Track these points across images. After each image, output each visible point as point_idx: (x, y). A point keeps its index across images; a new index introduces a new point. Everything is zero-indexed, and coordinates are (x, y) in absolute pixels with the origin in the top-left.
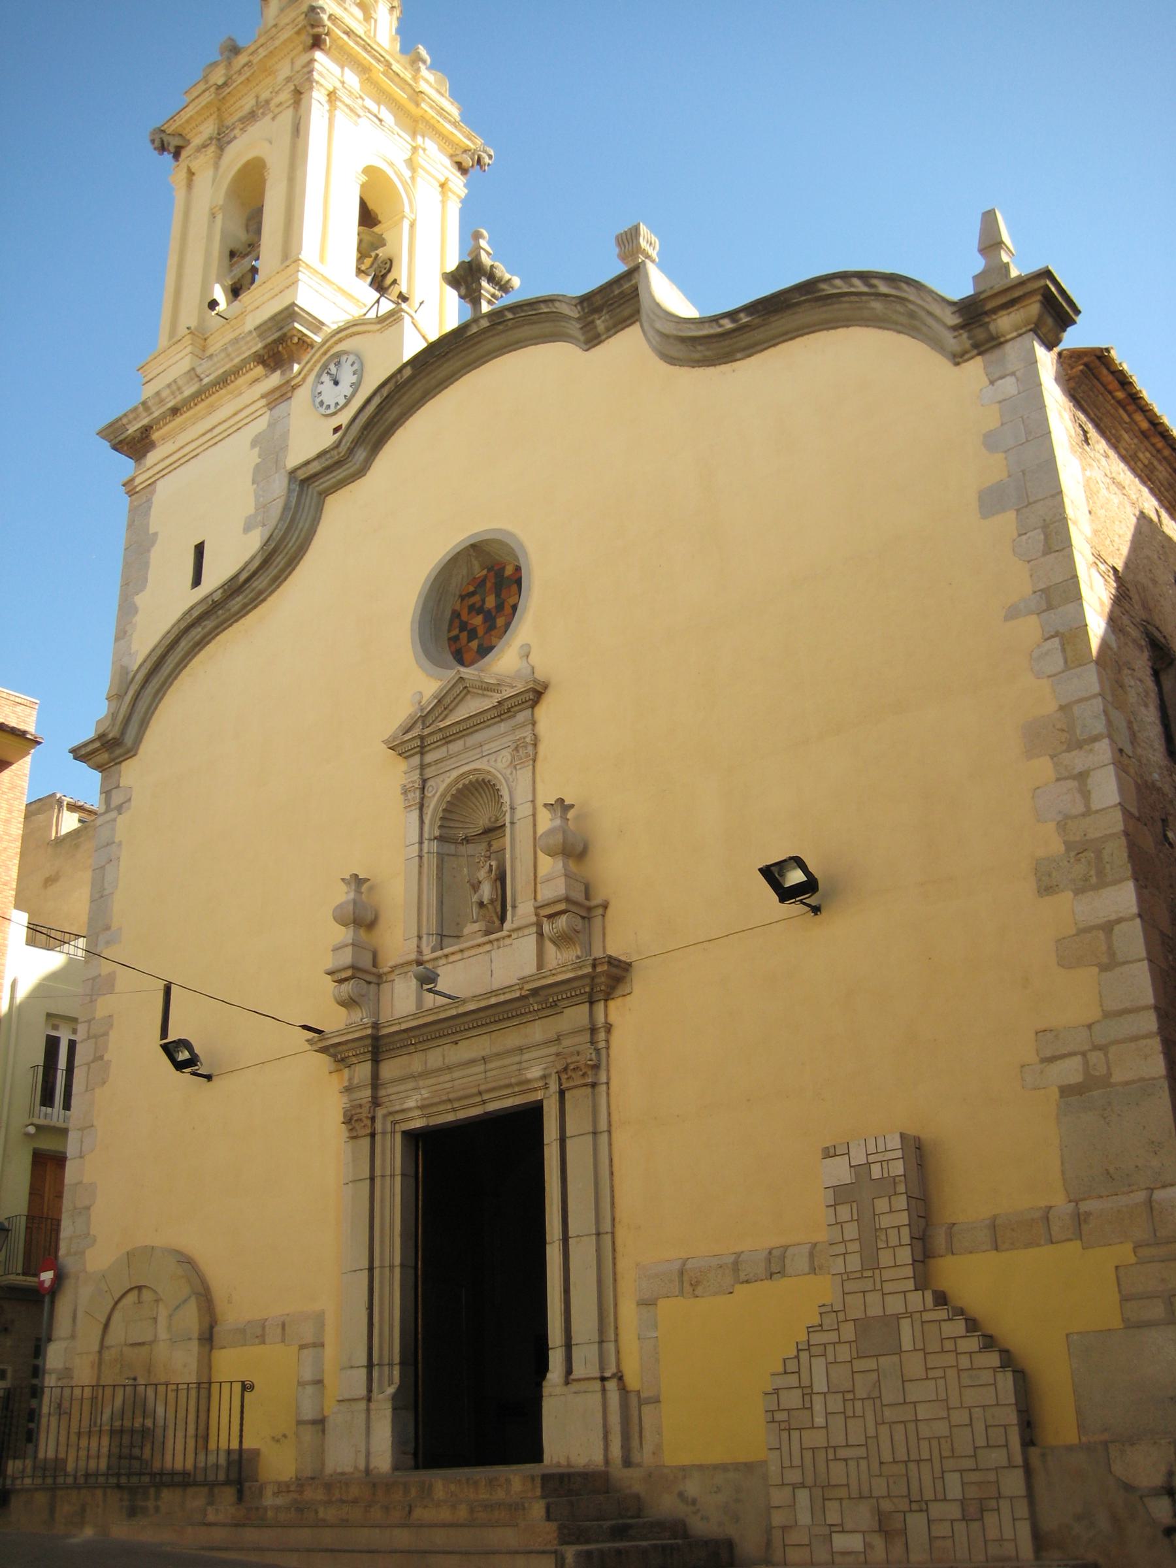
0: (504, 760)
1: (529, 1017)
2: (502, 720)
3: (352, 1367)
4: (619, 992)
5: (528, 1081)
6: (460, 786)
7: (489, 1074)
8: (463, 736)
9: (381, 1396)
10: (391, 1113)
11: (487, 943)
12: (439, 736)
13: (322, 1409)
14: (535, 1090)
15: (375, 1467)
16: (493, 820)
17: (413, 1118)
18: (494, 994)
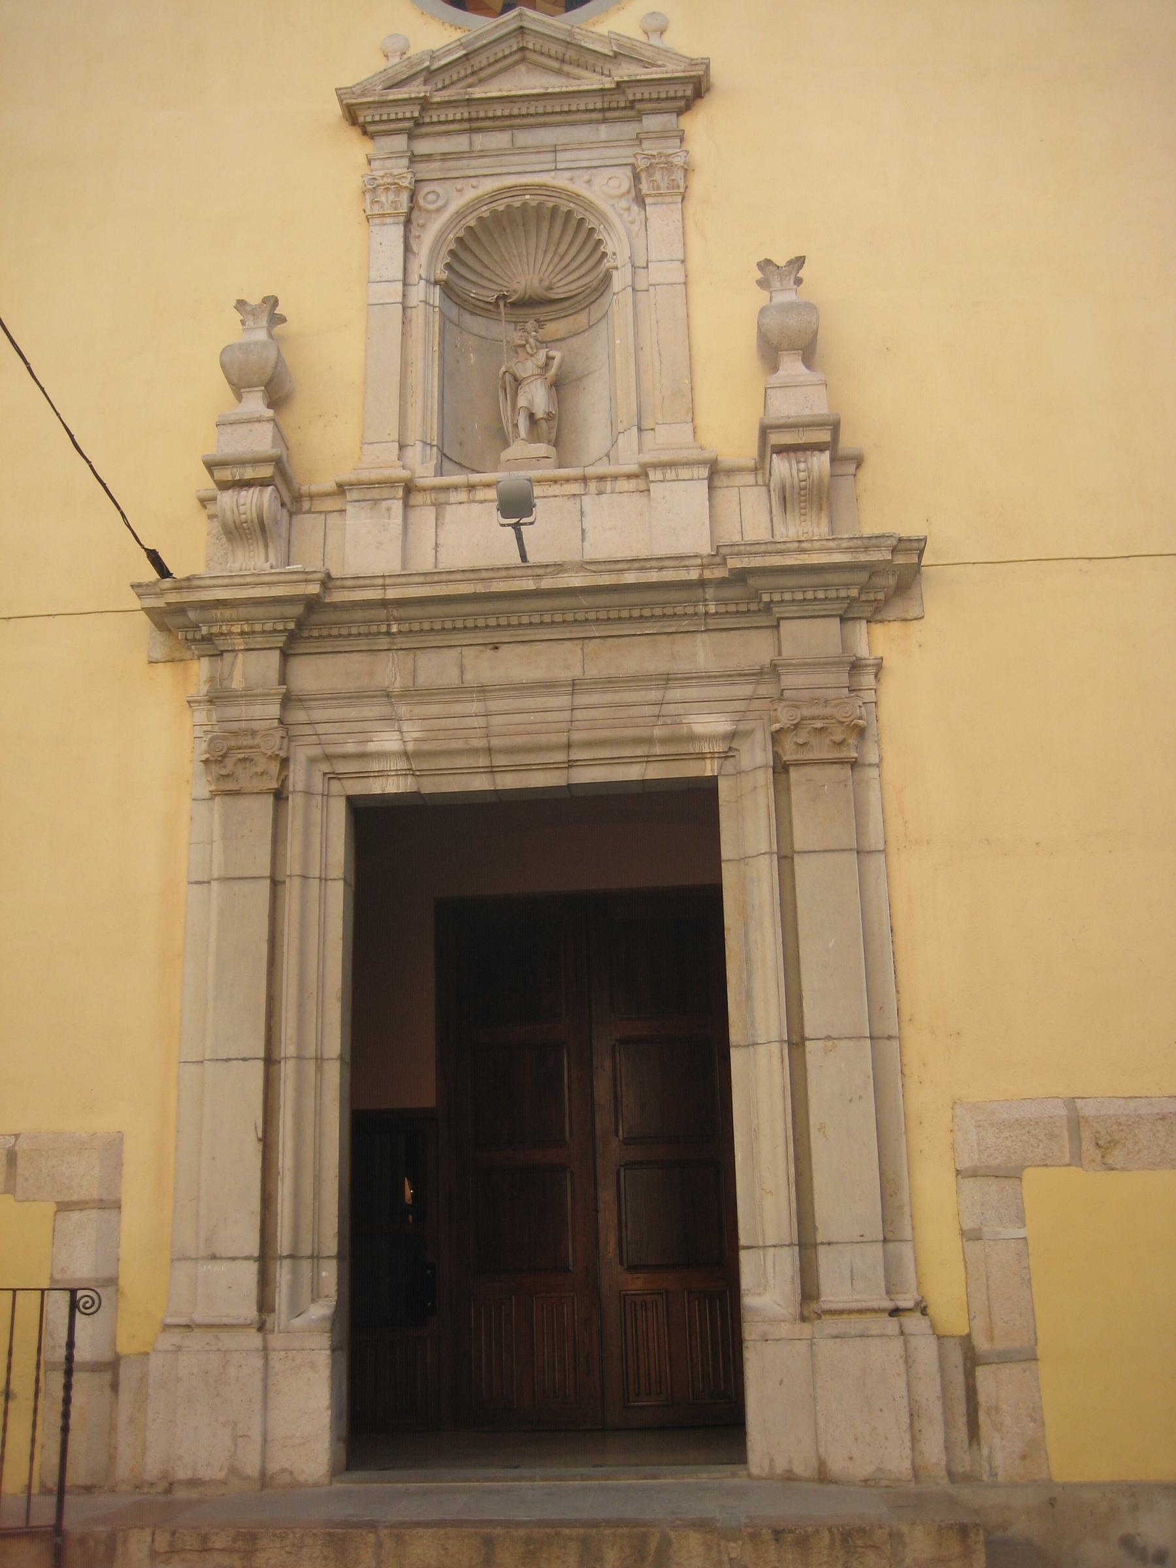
0: (613, 183)
1: (685, 625)
2: (605, 121)
3: (214, 1257)
4: (895, 610)
5: (692, 738)
6: (500, 206)
7: (579, 714)
8: (511, 127)
9: (298, 1322)
10: (328, 757)
11: (576, 480)
12: (462, 113)
13: (114, 1341)
14: (701, 757)
15: (283, 1470)
16: (546, 284)
17: (381, 774)
18: (637, 565)
